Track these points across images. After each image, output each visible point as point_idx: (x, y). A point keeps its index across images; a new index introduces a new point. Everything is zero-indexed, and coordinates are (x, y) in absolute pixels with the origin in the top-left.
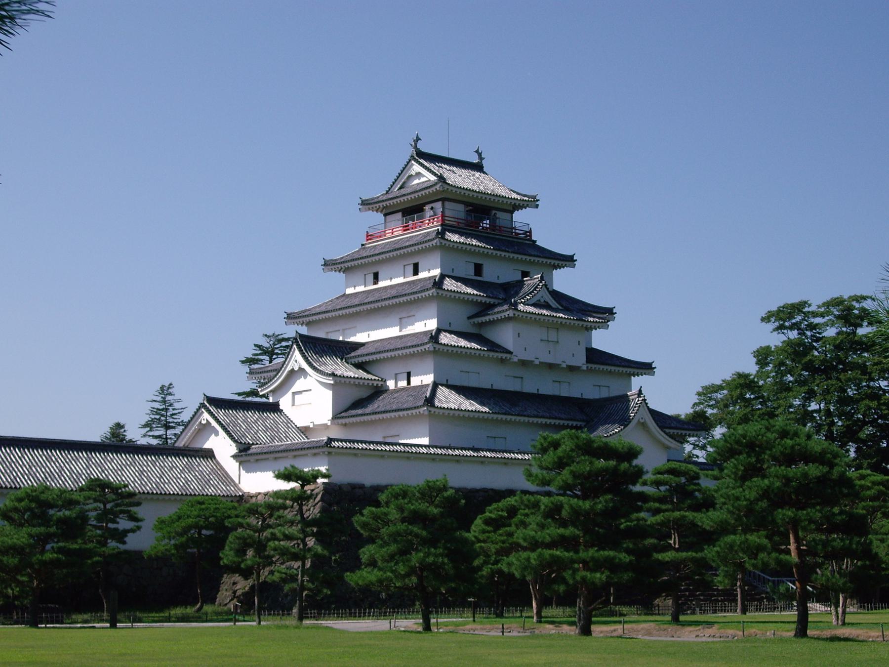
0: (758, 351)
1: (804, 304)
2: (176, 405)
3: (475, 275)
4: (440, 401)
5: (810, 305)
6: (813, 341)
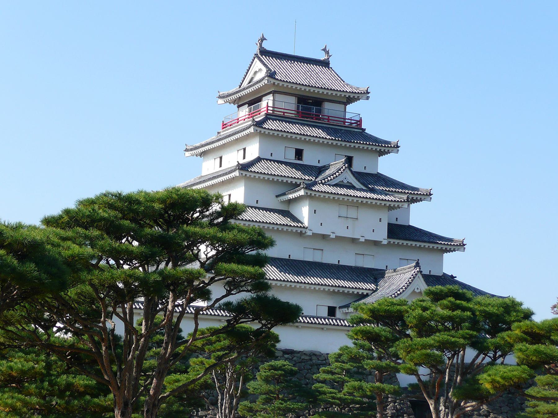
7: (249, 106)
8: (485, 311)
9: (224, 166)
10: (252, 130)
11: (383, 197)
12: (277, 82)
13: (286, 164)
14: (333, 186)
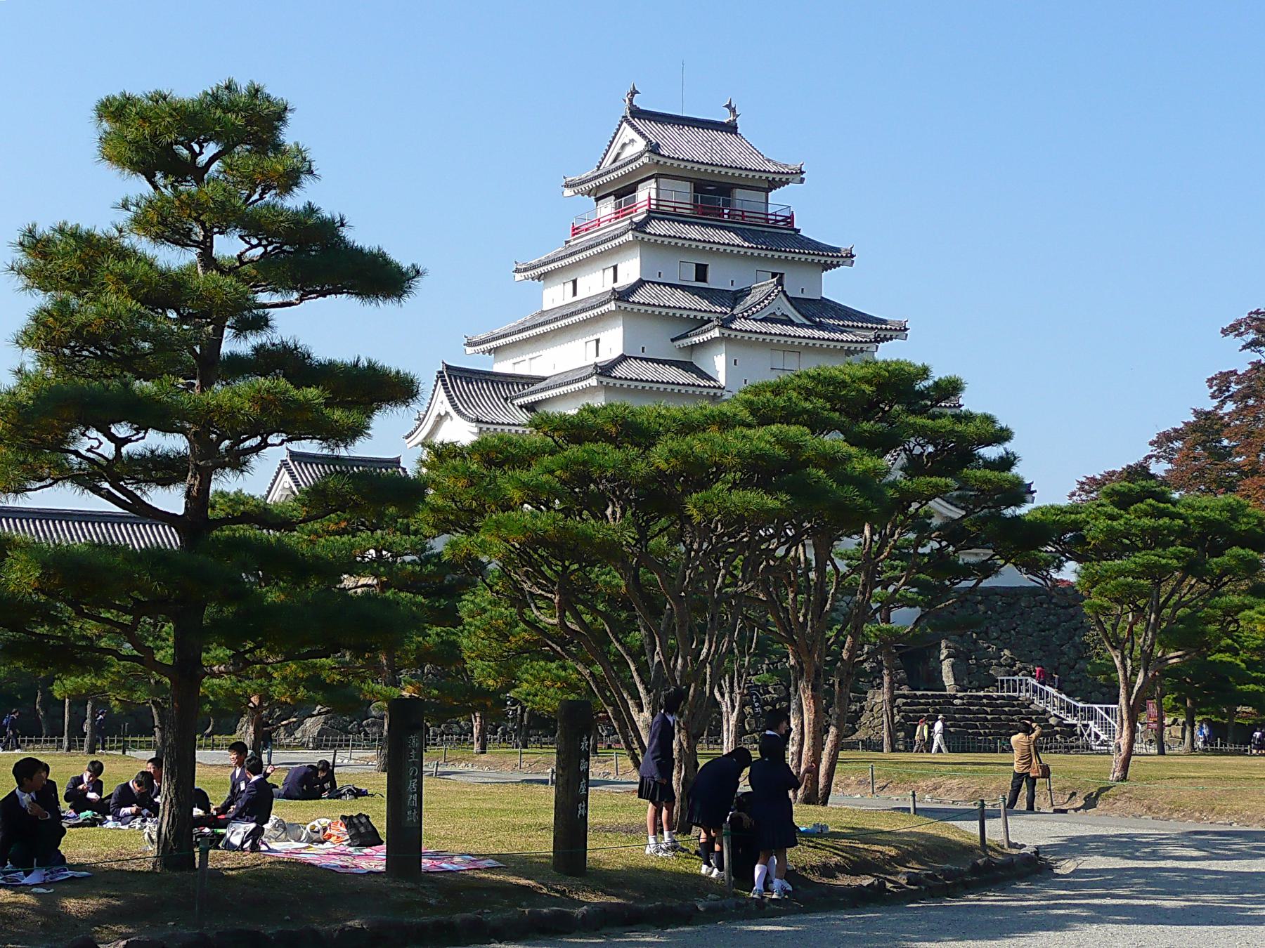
3: (697, 280)
7: (617, 198)
8: (1203, 518)
9: (580, 296)
10: (629, 236)
11: (837, 336)
12: (662, 160)
13: (683, 288)
14: (761, 320)
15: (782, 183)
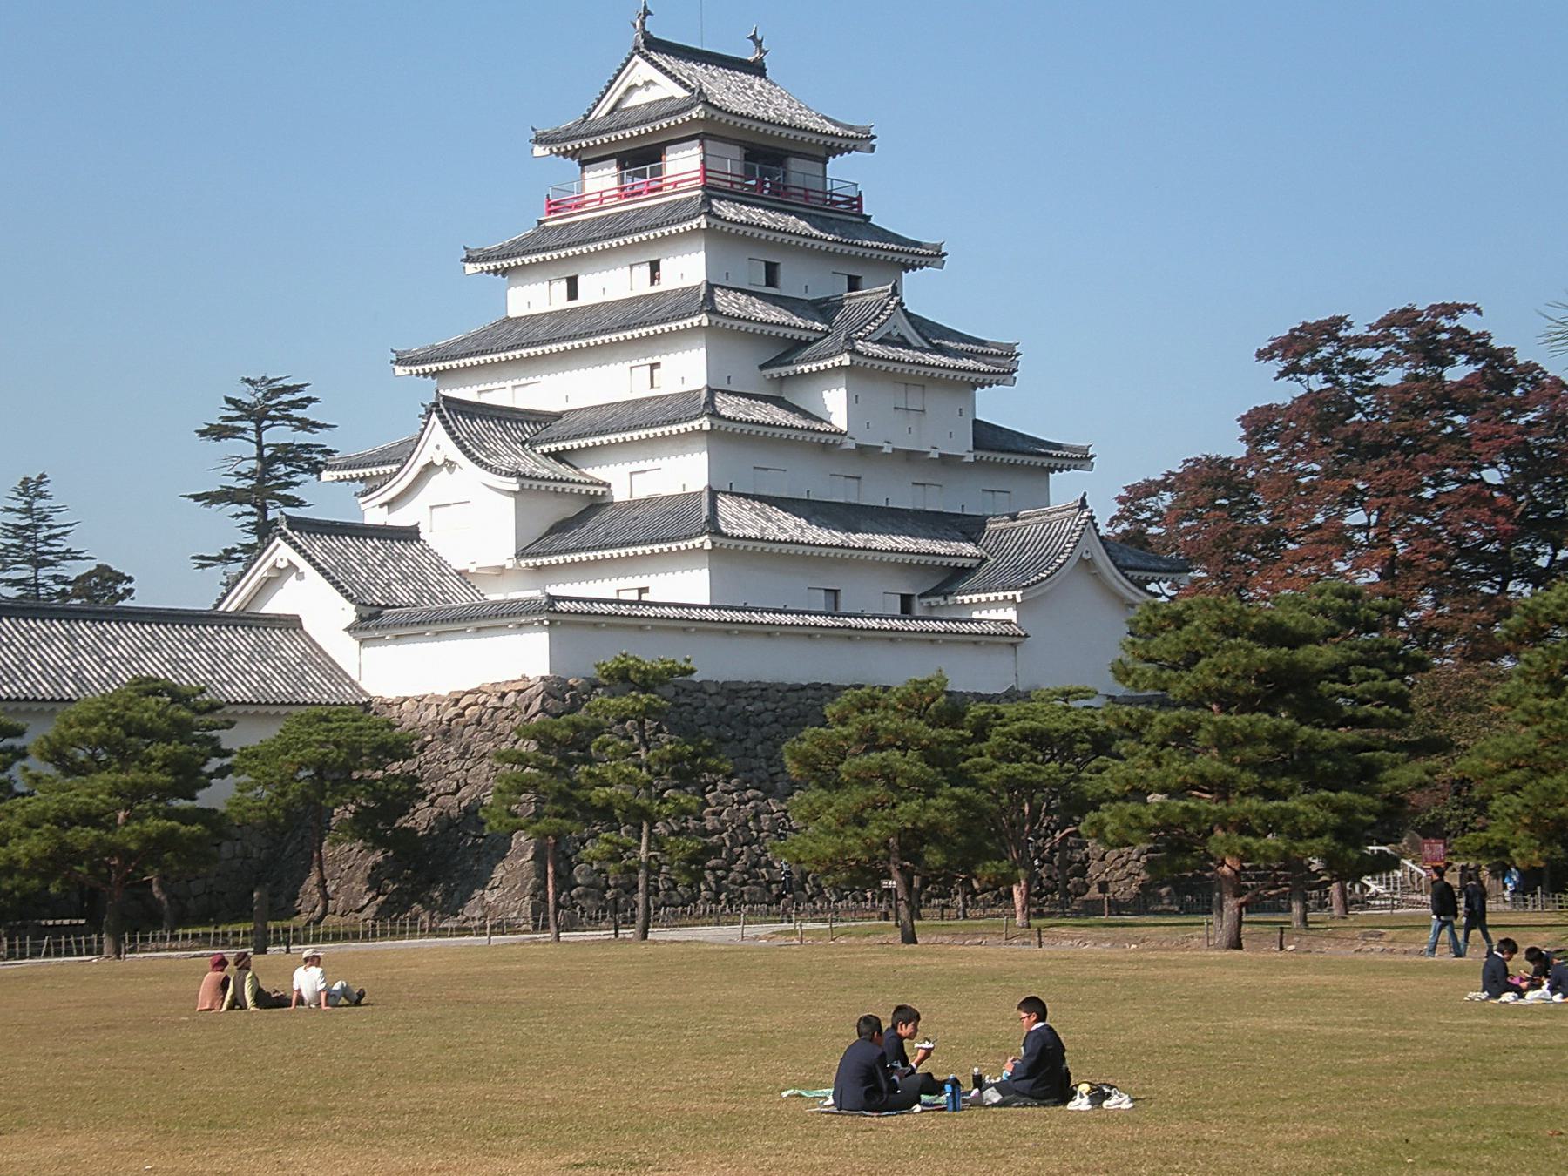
0: (1250, 414)
1: (1339, 322)
2: (56, 519)
4: (728, 523)
5: (1349, 325)
6: (1356, 393)
15: (841, 151)
